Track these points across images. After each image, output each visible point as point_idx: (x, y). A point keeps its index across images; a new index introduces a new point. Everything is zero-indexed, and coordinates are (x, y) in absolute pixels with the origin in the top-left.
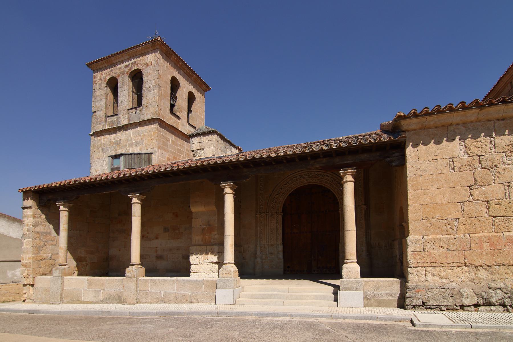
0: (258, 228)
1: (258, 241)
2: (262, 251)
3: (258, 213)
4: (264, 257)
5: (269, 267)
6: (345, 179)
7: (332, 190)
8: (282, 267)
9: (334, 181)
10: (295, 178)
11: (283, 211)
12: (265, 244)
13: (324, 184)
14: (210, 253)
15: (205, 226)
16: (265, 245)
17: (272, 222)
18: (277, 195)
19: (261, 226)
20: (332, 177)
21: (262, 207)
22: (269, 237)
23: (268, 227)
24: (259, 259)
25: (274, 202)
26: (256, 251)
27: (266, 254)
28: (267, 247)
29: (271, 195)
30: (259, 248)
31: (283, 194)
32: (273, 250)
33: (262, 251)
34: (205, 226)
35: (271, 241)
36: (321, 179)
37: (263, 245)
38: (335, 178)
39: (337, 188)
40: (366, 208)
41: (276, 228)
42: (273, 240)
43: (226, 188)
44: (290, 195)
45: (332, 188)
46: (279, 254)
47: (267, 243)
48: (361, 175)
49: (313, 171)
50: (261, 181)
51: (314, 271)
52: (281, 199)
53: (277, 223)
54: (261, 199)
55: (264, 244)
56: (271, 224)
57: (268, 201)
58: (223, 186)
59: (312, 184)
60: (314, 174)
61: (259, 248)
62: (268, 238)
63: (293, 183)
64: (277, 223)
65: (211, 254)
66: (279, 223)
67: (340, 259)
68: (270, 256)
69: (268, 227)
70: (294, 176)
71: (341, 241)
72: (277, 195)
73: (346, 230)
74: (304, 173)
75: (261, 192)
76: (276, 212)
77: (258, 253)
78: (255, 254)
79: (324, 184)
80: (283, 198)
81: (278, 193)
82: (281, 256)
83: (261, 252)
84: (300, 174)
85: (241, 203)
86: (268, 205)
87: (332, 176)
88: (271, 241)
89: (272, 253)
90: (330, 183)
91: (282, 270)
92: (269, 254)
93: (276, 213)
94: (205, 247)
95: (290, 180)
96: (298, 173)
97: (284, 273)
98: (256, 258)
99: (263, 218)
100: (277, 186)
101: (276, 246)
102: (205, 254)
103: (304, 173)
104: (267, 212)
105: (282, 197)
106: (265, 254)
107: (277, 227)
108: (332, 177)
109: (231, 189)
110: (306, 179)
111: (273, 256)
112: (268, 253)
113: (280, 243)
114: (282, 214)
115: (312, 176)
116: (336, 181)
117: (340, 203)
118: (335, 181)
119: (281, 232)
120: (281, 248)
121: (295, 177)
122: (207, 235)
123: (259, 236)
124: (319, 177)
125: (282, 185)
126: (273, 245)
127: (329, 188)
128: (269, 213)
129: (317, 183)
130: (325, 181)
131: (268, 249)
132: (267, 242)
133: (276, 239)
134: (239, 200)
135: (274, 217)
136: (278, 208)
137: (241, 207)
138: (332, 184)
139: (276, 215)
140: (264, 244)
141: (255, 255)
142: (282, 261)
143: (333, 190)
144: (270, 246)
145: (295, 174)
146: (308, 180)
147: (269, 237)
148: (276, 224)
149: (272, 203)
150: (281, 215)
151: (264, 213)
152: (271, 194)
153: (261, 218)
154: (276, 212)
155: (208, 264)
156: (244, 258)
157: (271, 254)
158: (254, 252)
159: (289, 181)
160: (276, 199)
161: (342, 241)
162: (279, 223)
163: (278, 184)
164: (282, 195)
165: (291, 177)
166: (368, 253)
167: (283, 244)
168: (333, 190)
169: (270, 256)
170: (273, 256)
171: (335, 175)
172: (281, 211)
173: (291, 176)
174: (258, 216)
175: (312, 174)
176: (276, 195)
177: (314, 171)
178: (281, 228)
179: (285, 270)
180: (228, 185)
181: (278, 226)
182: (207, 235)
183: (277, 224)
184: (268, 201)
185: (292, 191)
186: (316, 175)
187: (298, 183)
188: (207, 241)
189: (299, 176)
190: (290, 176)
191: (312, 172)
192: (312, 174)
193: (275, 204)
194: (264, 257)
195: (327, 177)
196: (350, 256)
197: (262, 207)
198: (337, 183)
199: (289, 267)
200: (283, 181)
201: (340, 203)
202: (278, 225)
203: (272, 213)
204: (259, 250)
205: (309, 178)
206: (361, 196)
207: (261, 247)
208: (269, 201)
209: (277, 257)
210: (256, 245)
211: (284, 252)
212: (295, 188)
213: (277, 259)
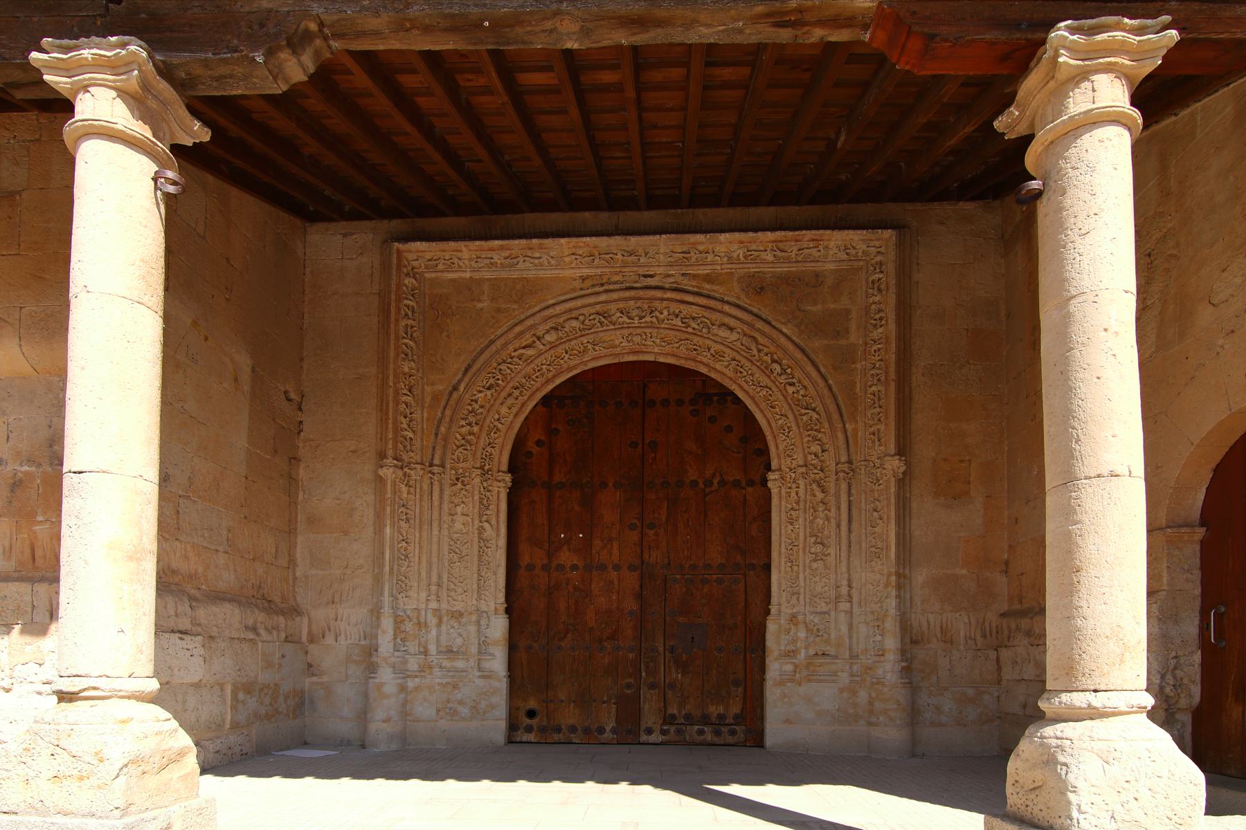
0: (388, 530)
1: (386, 593)
2: (403, 640)
3: (389, 461)
4: (413, 664)
5: (438, 711)
6: (1079, 102)
7: (740, 395)
8: (501, 712)
9: (755, 352)
10: (575, 324)
11: (512, 469)
12: (423, 606)
13: (707, 365)
14: (17, 628)
15: (26, 468)
16: (423, 613)
17: (459, 509)
18: (489, 393)
19: (403, 524)
20: (745, 335)
21: (410, 435)
22: (440, 577)
23: (435, 532)
24: (386, 676)
25: (474, 420)
26: (376, 637)
27: (426, 653)
28: (433, 621)
29: (455, 388)
30: (387, 623)
31: (516, 388)
32: (460, 635)
33: (403, 640)
34: (26, 468)
35: (452, 594)
36: (696, 339)
37: (408, 612)
38: (761, 339)
39: (765, 381)
40: (903, 469)
41: (480, 538)
42: (460, 590)
43: (85, 89)
44: (546, 400)
45: (744, 384)
46: (492, 655)
47: (433, 605)
48: (880, 330)
49: (662, 299)
50: (407, 315)
51: (649, 731)
52: (504, 410)
53: (480, 516)
54: (405, 398)
55: (418, 610)
56: (453, 521)
57: (443, 413)
58: (56, 68)
59: (650, 358)
60: (666, 313)
61: (387, 623)
62: (434, 579)
63: (566, 346)
64: (485, 518)
65: (23, 632)
66: (494, 522)
67: (769, 684)
68: (446, 663)
69: (435, 532)
70: (571, 310)
71: (773, 609)
72: (489, 389)
73: (1086, 467)
74: (621, 305)
75: (406, 370)
76: (482, 468)
77: (385, 643)
78: (371, 650)
79: (707, 365)
80: (514, 410)
81: (492, 381)
82: (498, 663)
83: (398, 640)
84: (598, 308)
85: (300, 409)
86: (443, 429)
87: (745, 328)
88: (452, 594)
89: (455, 650)
90: (738, 357)
91: (503, 725)
92: (439, 652)
93: (479, 472)
94: (24, 588)
95: (552, 328)
96: (592, 300)
97: (510, 741)
98: (372, 668)
99: (412, 490)
100: (487, 347)
101: (474, 618)
102: (23, 632)
103: (621, 305)
104: (436, 461)
105: (510, 401)
106: (420, 653)
107: (480, 533)
108: (745, 335)
109: (138, 102)
110: (626, 332)
111: (460, 664)
112: (432, 648)
113: (496, 609)
114: (508, 478)
115: (654, 320)
116: (766, 350)
117: (777, 448)
118: (759, 351)
119: (499, 556)
120: (498, 627)
121: (577, 319)
122: (40, 518)
123: (391, 569)
124: (690, 330)
125: (511, 347)
126: (461, 615)
127: (727, 383)
128: (442, 466)
129: (674, 355)
130: (712, 351)
131: (434, 632)
132: (433, 597)
133: (475, 586)
134: (293, 396)
135: (468, 487)
136: (489, 449)
137: (301, 431)
138: (743, 361)
139: (477, 480)
140: (418, 610)
141: (368, 657)
142: (502, 685)
143: (747, 393)
144: (445, 619)
145: (579, 303)
146: (637, 339)
147: (440, 577)
148: (476, 522)
149: (463, 423)
150: (501, 484)
151: (418, 467)
152: (459, 382)
153: (404, 489)
154: (482, 468)
155: (40, 693)
156: (310, 666)
157: (449, 652)
158: (363, 642)
159: (548, 332)
160: (482, 407)
161: (779, 611)
162: (494, 522)
163: (492, 342)
164: (510, 395)
165: (556, 316)
166: (903, 664)
167: (507, 611)
168: (747, 393)
169: (446, 663)
170: (460, 664)
171: (760, 325)
172: (505, 467)
173: (558, 309)
174: (388, 473)
175: (657, 313)
176: (480, 392)
177: (668, 299)
178: (502, 542)
179: (512, 727)
180: (99, 65)
181: (489, 532)
182: (40, 518)
183: (481, 522)
184: (439, 414)
185: (558, 381)
186: (677, 316)
187: (590, 346)
188: (39, 553)
189: (597, 313)
190: (551, 311)
191: (657, 304)
192: (657, 313)
193: (476, 429)
194: (413, 664)
195: (723, 333)
196: (1122, 661)
197: (410, 435)
198: (768, 359)
199: (531, 714)
200: (518, 329)
201: (777, 448)
202: (486, 525)
203: (461, 471)
204: (391, 632)
205: (639, 331)
206: (879, 420)
207: (398, 622)
208: (448, 412)
209: (480, 669)
210: (376, 612)
211: (512, 648)
212: (575, 372)
213: (480, 677)
